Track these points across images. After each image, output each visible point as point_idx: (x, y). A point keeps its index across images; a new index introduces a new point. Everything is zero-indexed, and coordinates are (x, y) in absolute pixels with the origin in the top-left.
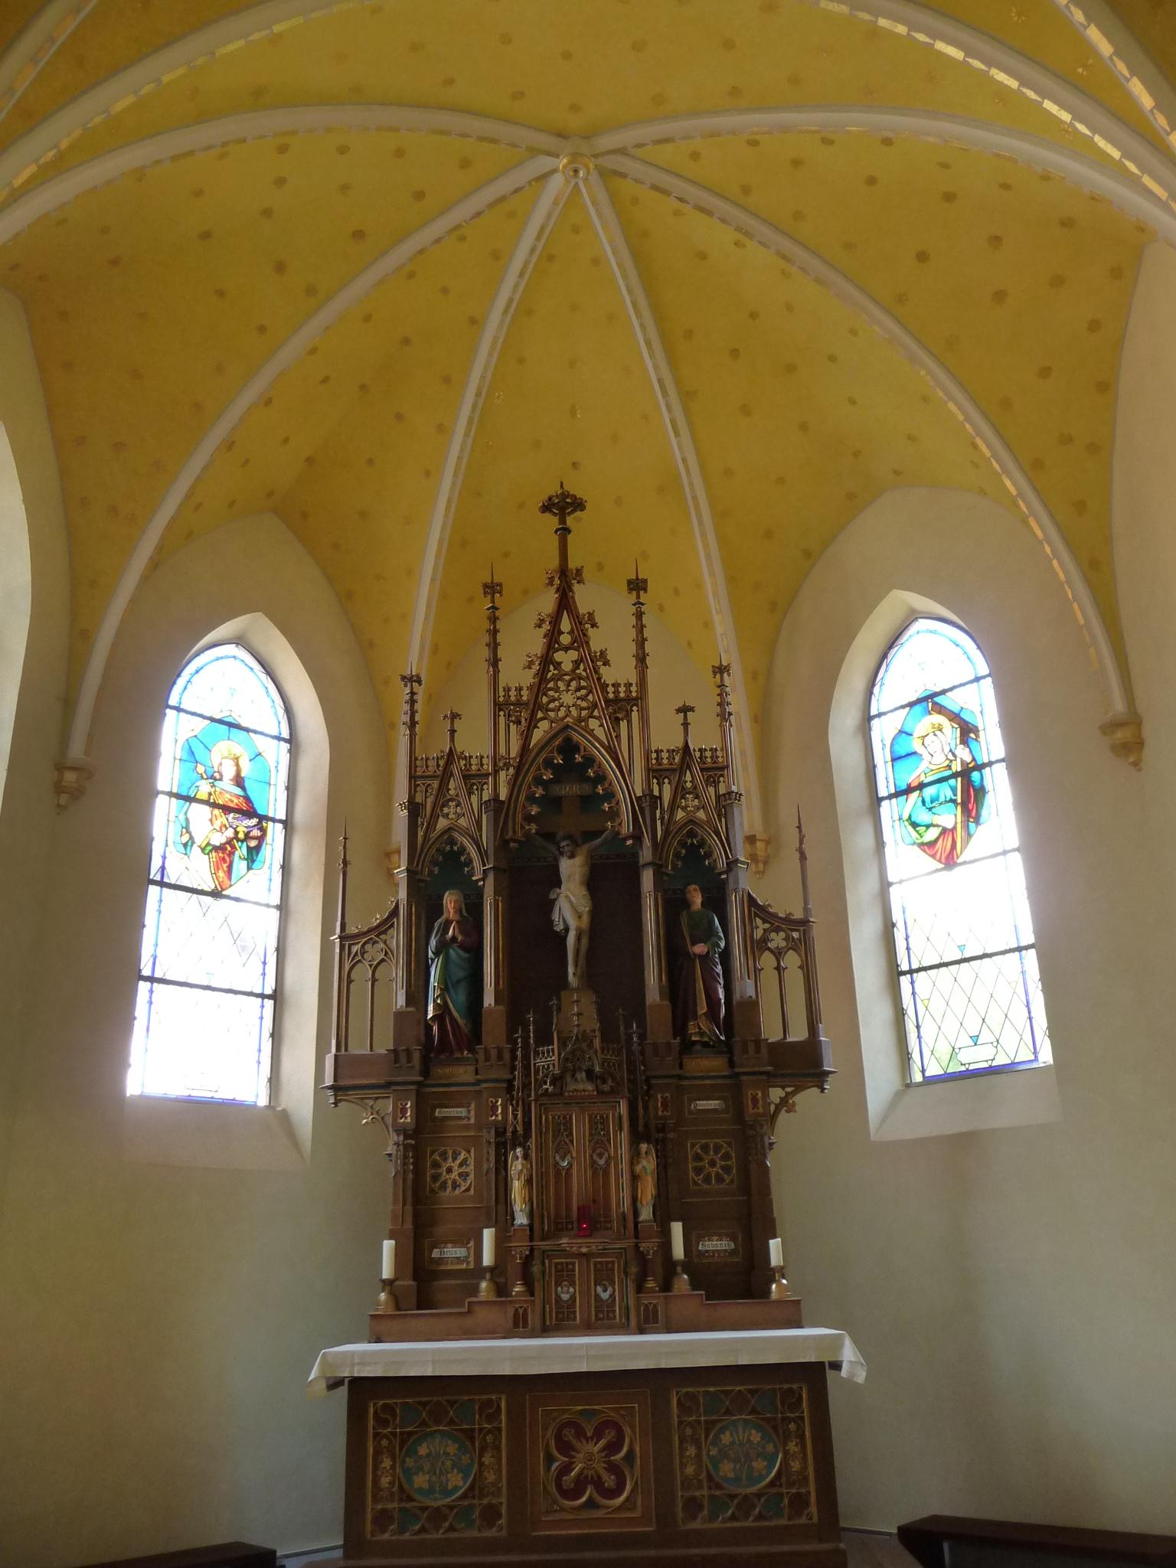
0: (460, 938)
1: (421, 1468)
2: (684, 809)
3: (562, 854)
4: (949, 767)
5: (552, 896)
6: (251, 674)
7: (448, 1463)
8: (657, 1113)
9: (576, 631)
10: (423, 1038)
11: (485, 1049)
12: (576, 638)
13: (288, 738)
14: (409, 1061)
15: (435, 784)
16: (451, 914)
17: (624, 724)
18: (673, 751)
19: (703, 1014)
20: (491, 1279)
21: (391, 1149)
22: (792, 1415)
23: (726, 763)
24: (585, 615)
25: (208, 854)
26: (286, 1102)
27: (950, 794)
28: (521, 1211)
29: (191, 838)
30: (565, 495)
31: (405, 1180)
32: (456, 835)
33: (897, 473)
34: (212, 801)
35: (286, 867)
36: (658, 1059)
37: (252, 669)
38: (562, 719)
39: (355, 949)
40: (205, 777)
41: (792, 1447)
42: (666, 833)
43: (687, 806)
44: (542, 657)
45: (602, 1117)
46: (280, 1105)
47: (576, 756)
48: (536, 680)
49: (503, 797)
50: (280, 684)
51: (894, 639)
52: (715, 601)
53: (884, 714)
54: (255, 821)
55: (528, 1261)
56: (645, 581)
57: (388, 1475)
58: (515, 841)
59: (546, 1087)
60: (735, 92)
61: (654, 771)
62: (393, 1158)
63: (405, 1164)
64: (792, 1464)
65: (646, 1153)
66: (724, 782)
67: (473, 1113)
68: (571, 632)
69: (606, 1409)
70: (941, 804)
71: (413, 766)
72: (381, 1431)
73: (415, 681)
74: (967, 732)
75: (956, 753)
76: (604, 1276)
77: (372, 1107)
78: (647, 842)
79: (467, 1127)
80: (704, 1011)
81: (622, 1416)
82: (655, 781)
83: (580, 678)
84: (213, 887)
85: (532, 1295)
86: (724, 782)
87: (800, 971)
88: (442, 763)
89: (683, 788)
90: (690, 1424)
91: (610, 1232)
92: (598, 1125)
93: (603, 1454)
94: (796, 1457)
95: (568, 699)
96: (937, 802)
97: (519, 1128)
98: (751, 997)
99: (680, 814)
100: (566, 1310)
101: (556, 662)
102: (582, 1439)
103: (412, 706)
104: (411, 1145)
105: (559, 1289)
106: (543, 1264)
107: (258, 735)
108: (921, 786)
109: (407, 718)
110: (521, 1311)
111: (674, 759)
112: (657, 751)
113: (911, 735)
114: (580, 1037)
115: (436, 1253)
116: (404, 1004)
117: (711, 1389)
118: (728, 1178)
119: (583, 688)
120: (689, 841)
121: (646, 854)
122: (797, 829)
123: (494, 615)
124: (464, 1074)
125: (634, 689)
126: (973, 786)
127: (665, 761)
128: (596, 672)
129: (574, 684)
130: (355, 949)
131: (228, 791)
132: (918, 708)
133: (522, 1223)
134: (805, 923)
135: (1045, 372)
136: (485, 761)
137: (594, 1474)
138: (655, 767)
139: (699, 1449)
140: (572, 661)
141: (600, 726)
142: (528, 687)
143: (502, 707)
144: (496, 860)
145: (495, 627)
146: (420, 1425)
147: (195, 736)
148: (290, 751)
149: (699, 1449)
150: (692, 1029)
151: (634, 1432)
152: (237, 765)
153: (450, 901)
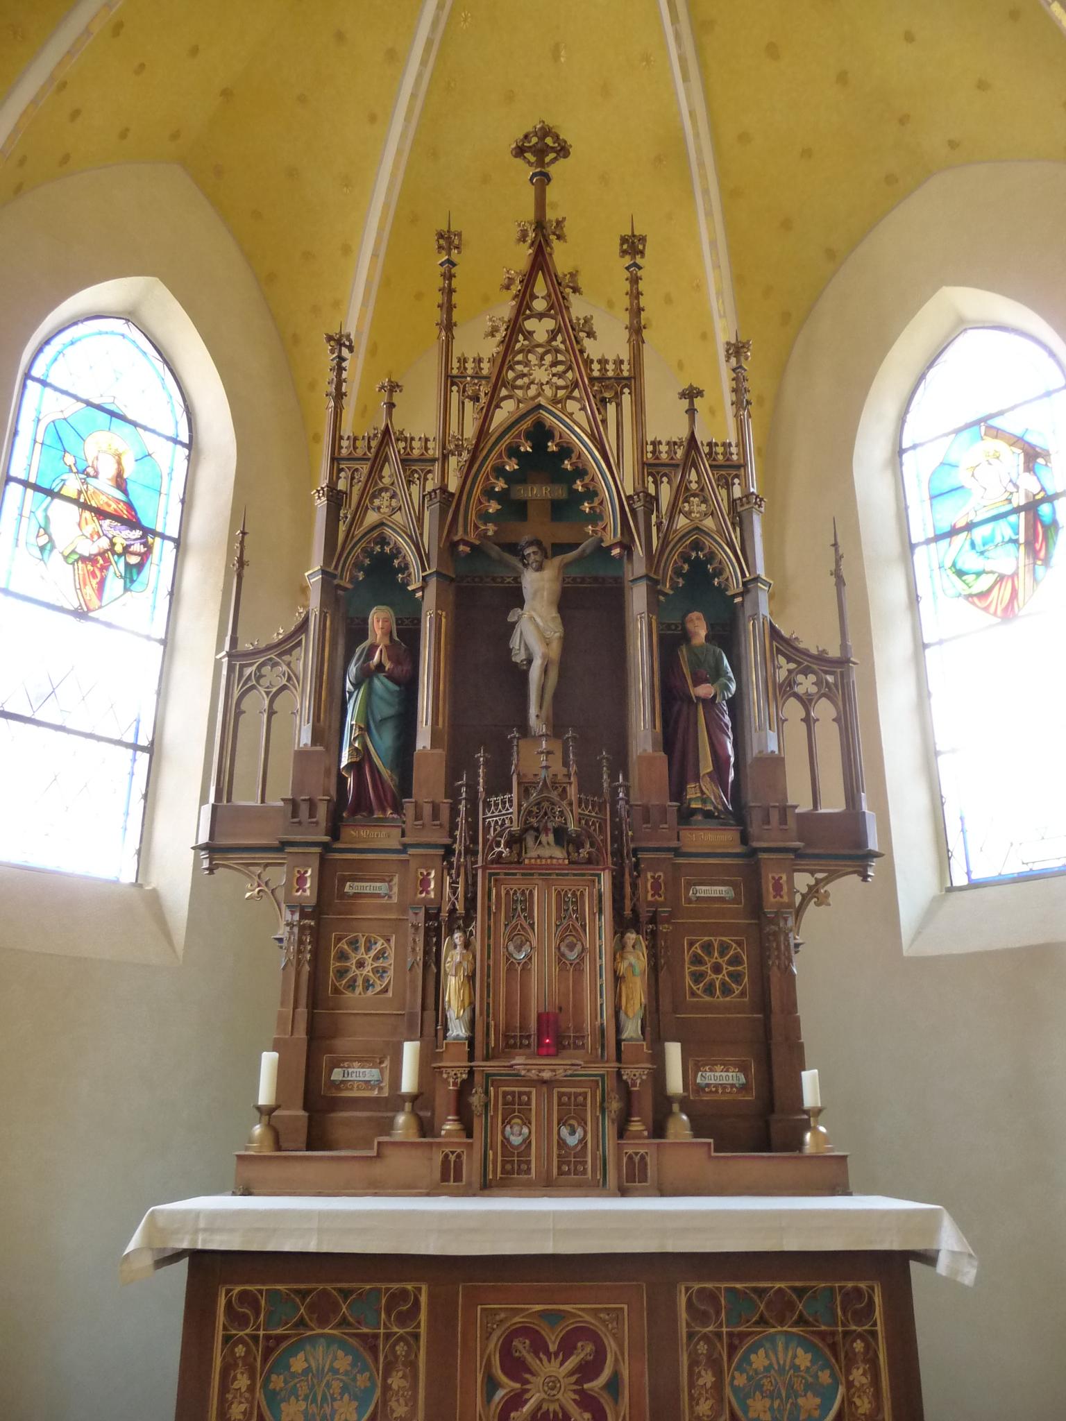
0: (388, 665)
1: (294, 1392)
2: (687, 515)
3: (526, 566)
4: (1009, 501)
5: (511, 618)
7: (336, 1386)
8: (646, 898)
9: (553, 295)
10: (333, 792)
11: (416, 802)
12: (553, 304)
13: (187, 442)
14: (312, 815)
15: (365, 468)
16: (378, 637)
17: (611, 408)
18: (675, 443)
19: (707, 773)
20: (413, 1112)
21: (283, 932)
22: (859, 1329)
23: (742, 462)
24: (566, 275)
25: (73, 564)
26: (157, 880)
27: (1009, 534)
28: (458, 1018)
29: (51, 540)
30: (545, 132)
31: (298, 974)
32: (388, 531)
33: (953, 145)
34: (82, 500)
35: (174, 594)
36: (649, 826)
38: (533, 398)
39: (248, 671)
40: (75, 470)
41: (859, 1375)
42: (664, 543)
43: (691, 512)
45: (574, 894)
46: (149, 884)
48: (502, 348)
49: (453, 486)
50: (181, 378)
52: (718, 302)
54: (138, 533)
55: (464, 1089)
56: (643, 239)
57: (243, 1400)
58: (466, 543)
59: (500, 849)
61: (650, 465)
62: (285, 944)
63: (299, 952)
64: (858, 1402)
65: (633, 947)
66: (739, 484)
67: (395, 889)
69: (579, 1311)
70: (997, 546)
72: (234, 1332)
75: (1018, 483)
76: (571, 1112)
77: (259, 876)
78: (639, 551)
79: (386, 908)
80: (709, 770)
81: (603, 1321)
82: (651, 479)
83: (557, 351)
84: (76, 605)
85: (470, 1134)
86: (739, 484)
87: (835, 725)
88: (374, 444)
89: (687, 489)
90: (705, 1338)
91: (582, 1052)
92: (568, 906)
93: (573, 1379)
94: (865, 1392)
95: (541, 375)
96: (991, 544)
97: (460, 907)
98: (773, 752)
99: (682, 522)
100: (516, 1159)
102: (541, 1355)
103: (339, 375)
104: (310, 926)
105: (508, 1128)
106: (487, 1092)
107: (147, 433)
108: (969, 527)
109: (332, 389)
110: (452, 1158)
111: (675, 453)
112: (653, 443)
113: (957, 467)
114: (548, 781)
115: (337, 1075)
116: (309, 742)
117: (738, 1286)
118: (737, 989)
119: (561, 363)
120: (694, 554)
121: (639, 566)
122: (833, 548)
123: (450, 271)
124: (387, 838)
125: (625, 367)
126: (1042, 522)
128: (578, 342)
129: (549, 358)
130: (248, 671)
131: (104, 492)
132: (965, 435)
133: (458, 1035)
134: (842, 663)
136: (430, 445)
137: (558, 1408)
138: (652, 461)
139: (719, 1374)
141: (580, 410)
143: (456, 380)
144: (439, 565)
145: (450, 284)
146: (296, 1326)
147: (65, 419)
148: (189, 458)
149: (719, 1374)
150: (692, 792)
151: (621, 1347)
152: (119, 463)
153: (379, 621)
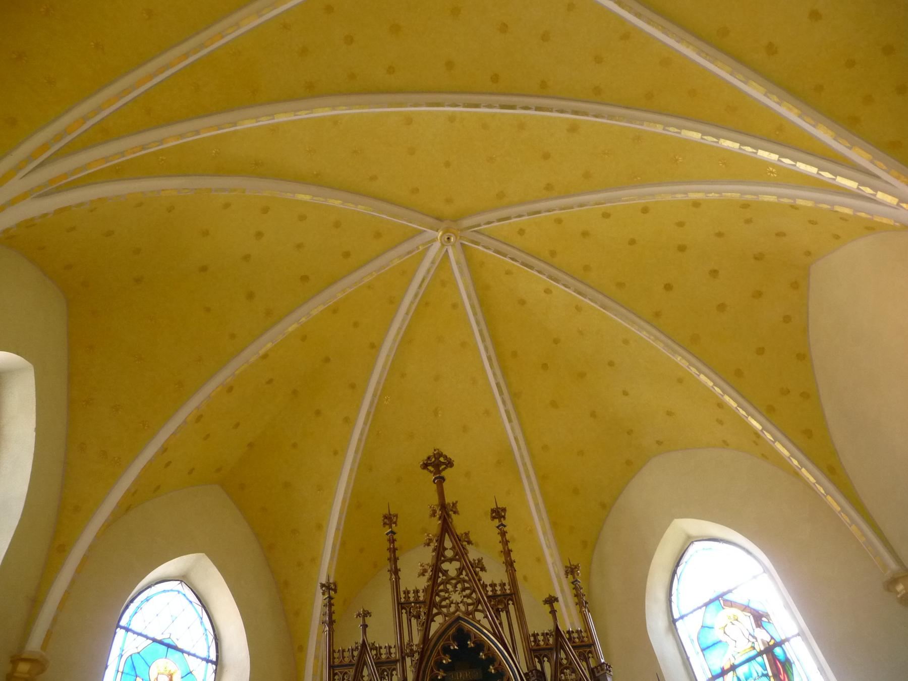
4: (754, 648)
6: (190, 605)
9: (456, 546)
15: (352, 672)
17: (503, 615)
18: (547, 634)
23: (591, 642)
24: (463, 534)
27: (760, 670)
33: (659, 443)
37: (191, 602)
44: (433, 565)
47: (469, 642)
48: (430, 583)
51: (678, 559)
53: (686, 615)
60: (549, 187)
61: (535, 651)
68: (453, 548)
71: (332, 658)
73: (332, 590)
74: (759, 618)
82: (537, 660)
83: (464, 581)
88: (356, 653)
89: (561, 664)
101: (444, 570)
119: (468, 588)
123: (393, 538)
125: (507, 587)
126: (779, 661)
127: (542, 643)
129: (459, 586)
132: (712, 607)
135: (760, 351)
136: (393, 650)
138: (535, 648)
140: (456, 569)
141: (484, 618)
142: (423, 590)
143: (404, 606)
148: (215, 671)
